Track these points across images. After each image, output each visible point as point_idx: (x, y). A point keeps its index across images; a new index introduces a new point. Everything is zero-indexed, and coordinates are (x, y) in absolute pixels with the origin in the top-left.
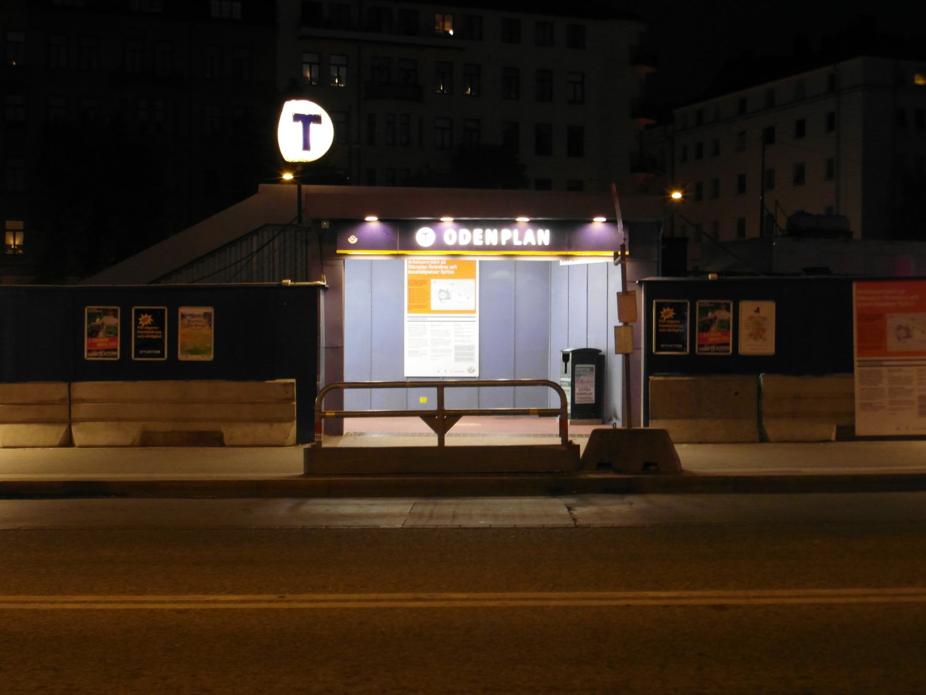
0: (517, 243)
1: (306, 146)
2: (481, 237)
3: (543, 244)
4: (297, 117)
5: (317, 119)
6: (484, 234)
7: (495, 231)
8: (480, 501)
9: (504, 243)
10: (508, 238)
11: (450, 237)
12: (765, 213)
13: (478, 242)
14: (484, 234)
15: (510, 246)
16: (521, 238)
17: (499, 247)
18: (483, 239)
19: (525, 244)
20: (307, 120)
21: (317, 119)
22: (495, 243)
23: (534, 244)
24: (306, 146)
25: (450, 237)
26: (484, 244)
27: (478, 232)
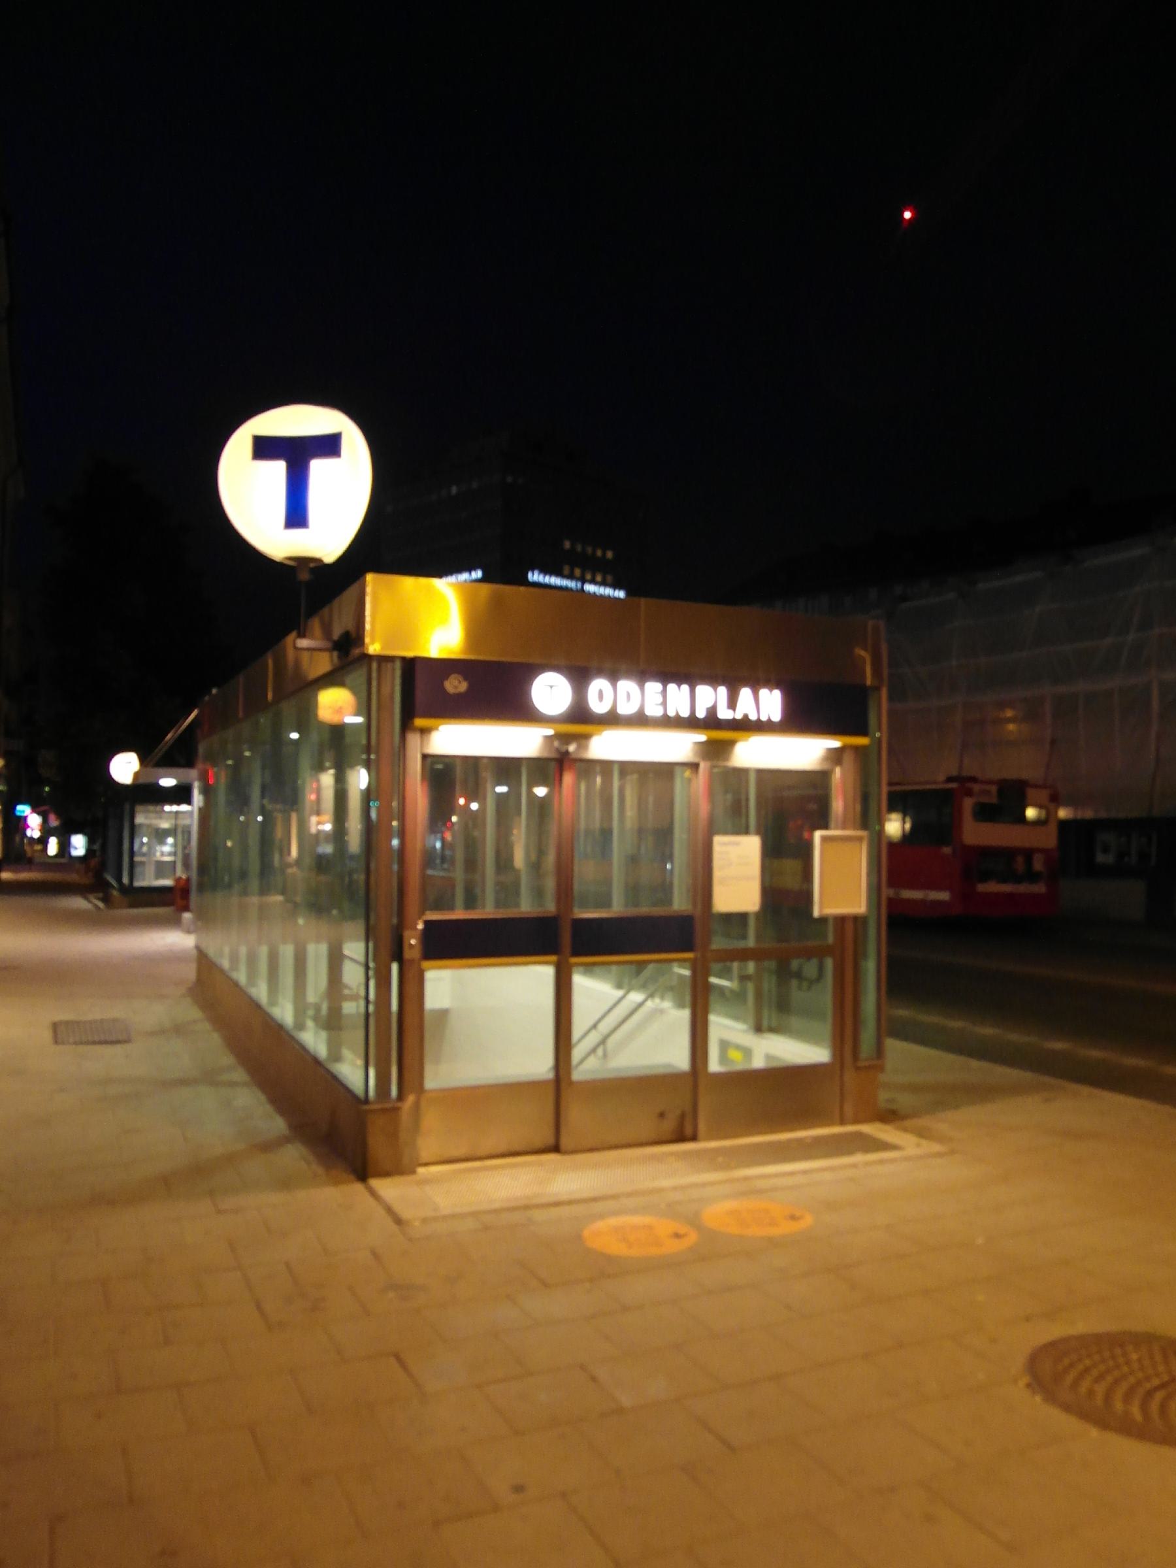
0: (724, 714)
1: (296, 516)
2: (660, 699)
3: (769, 720)
4: (265, 448)
5: (329, 445)
6: (664, 692)
7: (685, 688)
8: (484, 917)
9: (701, 714)
10: (710, 705)
11: (601, 695)
12: (553, 828)
13: (626, 709)
14: (664, 692)
15: (711, 722)
16: (732, 704)
17: (691, 723)
18: (664, 703)
19: (739, 716)
20: (297, 454)
21: (329, 445)
22: (685, 713)
23: (753, 717)
24: (296, 516)
25: (601, 695)
26: (665, 716)
27: (653, 687)
